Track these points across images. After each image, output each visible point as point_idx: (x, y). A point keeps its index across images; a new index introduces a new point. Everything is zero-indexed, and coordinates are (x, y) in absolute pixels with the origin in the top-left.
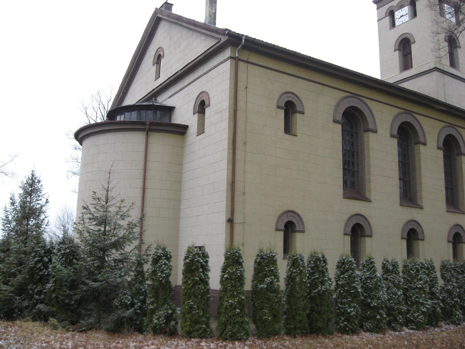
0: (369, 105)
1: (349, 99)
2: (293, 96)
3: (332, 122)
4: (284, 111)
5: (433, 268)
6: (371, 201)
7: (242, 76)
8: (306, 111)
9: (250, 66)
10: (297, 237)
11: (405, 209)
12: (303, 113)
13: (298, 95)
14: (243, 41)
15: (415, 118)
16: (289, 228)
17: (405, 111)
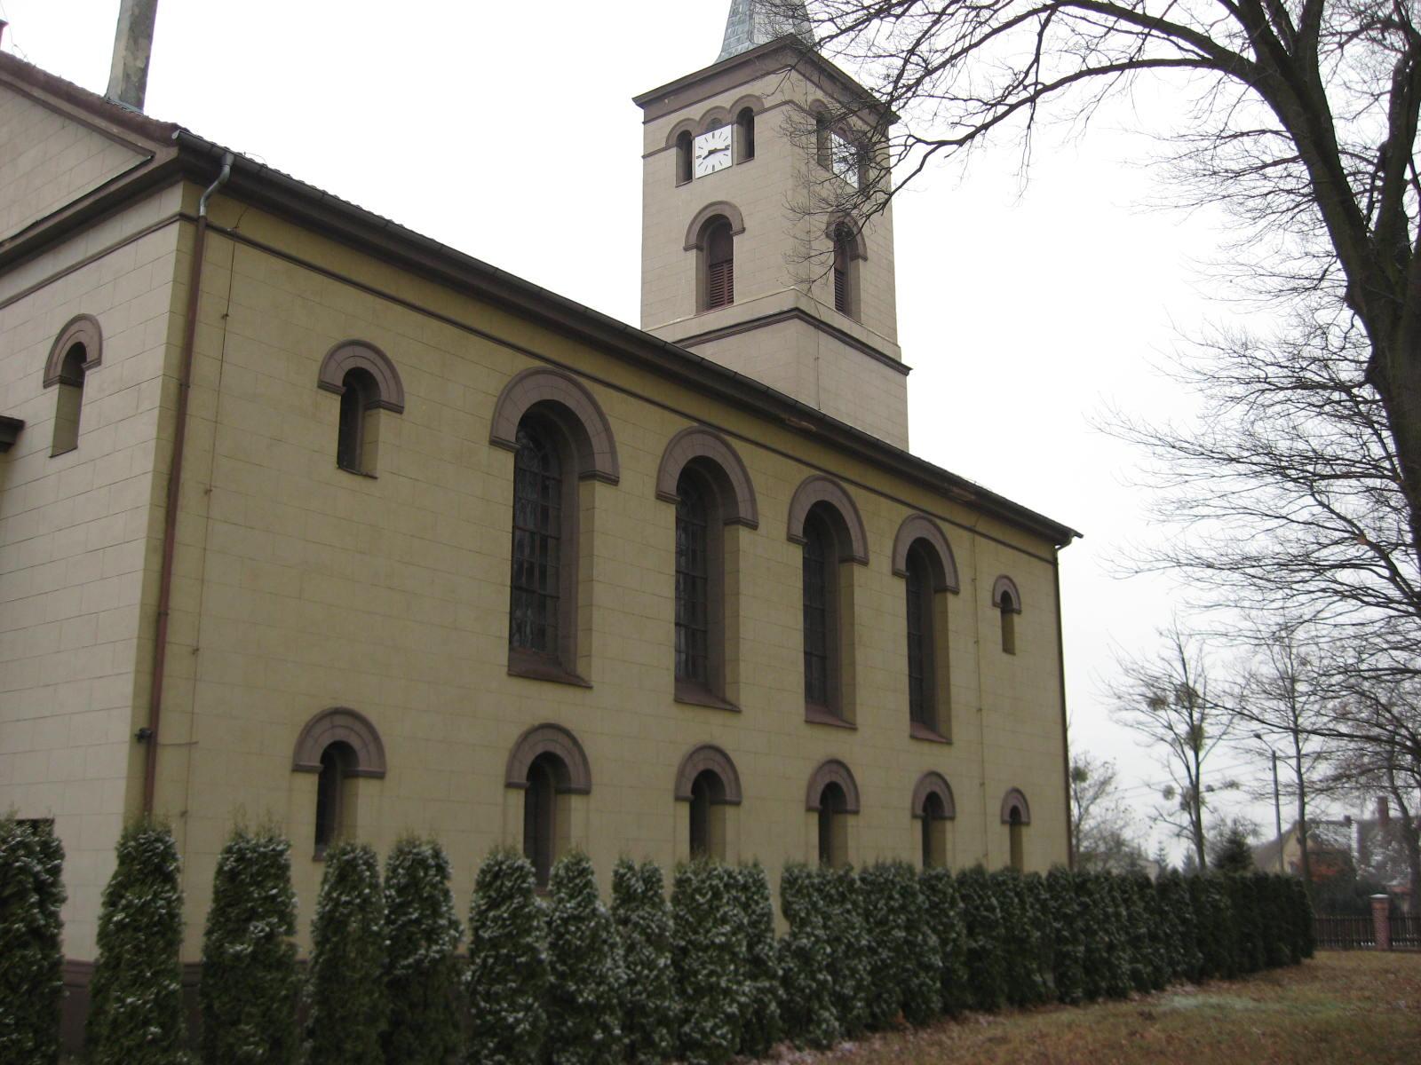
8: (409, 403)
9: (242, 249)
14: (227, 169)
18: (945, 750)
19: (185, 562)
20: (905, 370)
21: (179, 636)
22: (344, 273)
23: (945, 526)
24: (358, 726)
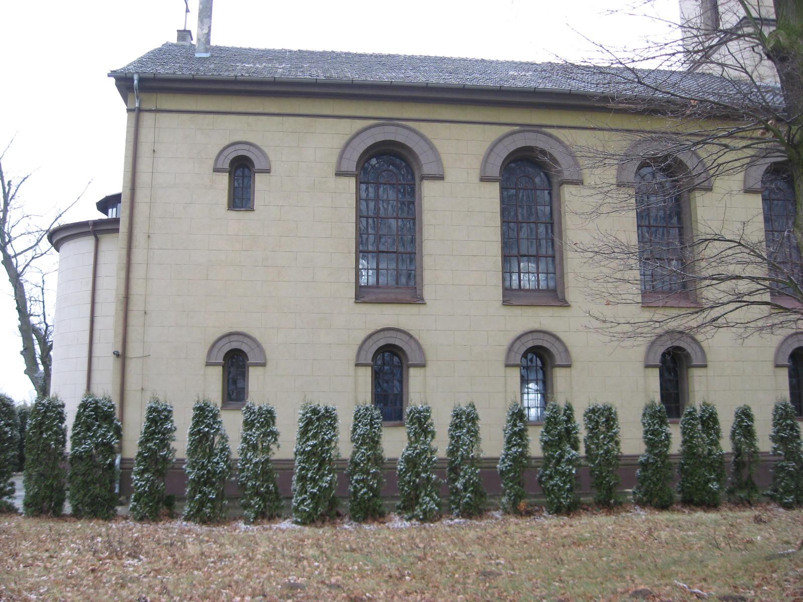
1: (516, 137)
3: (334, 176)
4: (228, 174)
6: (425, 304)
7: (146, 135)
8: (275, 167)
10: (558, 374)
11: (517, 311)
14: (136, 82)
15: (550, 136)
16: (236, 363)
17: (522, 129)
18: (422, 308)
19: (138, 273)
21: (136, 305)
22: (228, 110)
23: (423, 128)
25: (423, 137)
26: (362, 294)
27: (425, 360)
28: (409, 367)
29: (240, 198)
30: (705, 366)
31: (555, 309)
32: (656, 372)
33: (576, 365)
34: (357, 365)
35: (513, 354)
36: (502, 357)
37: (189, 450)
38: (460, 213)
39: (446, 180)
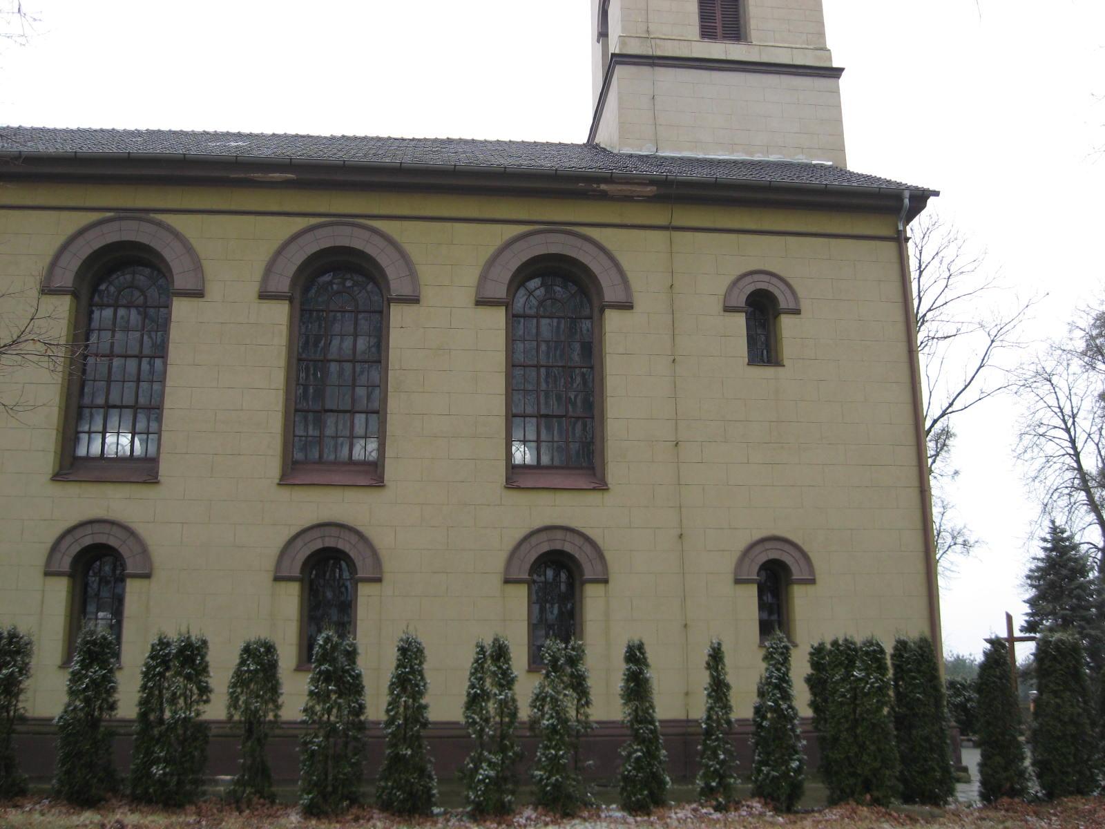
0: (396, 236)
2: (766, 278)
5: (882, 651)
9: (677, 235)
12: (797, 312)
13: (782, 274)
14: (907, 201)
15: (160, 224)
16: (774, 580)
20: (836, 73)
24: (787, 547)
25: (177, 235)
26: (515, 476)
27: (151, 569)
28: (584, 582)
29: (764, 348)
30: (379, 580)
31: (134, 488)
32: (753, 590)
33: (160, 574)
34: (277, 579)
35: (58, 556)
36: (40, 560)
37: (466, 703)
38: (228, 350)
39: (208, 297)
